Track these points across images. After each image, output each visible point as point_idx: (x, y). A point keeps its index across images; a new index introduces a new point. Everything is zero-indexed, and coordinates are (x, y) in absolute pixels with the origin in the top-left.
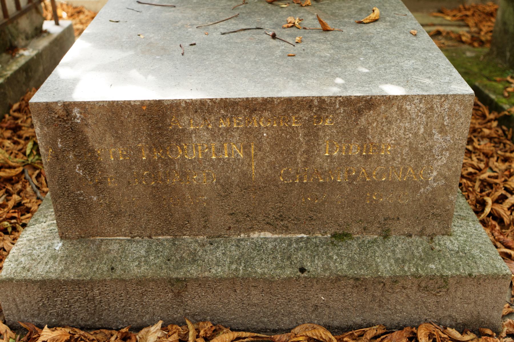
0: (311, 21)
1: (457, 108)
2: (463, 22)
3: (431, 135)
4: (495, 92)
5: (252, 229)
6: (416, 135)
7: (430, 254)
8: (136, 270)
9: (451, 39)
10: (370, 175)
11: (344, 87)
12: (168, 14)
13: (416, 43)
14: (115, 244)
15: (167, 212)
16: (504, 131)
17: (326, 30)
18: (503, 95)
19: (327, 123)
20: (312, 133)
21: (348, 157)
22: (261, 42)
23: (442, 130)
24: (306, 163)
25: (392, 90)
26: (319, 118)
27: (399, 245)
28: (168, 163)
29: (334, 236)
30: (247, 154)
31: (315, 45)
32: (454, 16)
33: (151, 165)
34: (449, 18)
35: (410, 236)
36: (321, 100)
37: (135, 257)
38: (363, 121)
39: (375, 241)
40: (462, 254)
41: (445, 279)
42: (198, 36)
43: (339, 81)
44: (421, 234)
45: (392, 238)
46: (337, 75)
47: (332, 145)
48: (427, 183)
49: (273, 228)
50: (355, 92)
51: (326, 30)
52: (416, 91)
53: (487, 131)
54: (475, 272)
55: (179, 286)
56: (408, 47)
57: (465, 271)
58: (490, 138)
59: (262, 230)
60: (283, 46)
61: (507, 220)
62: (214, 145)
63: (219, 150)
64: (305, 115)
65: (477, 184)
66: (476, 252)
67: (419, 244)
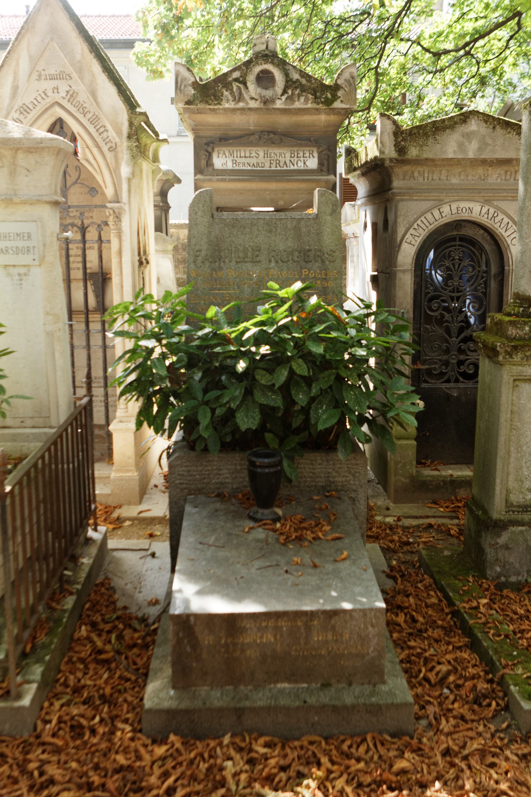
0: (307, 559)
1: (378, 614)
2: (454, 515)
3: (367, 628)
4: (454, 591)
5: (277, 681)
6: (360, 628)
7: (373, 694)
8: (217, 704)
9: (442, 532)
10: (339, 649)
11: (323, 604)
12: (221, 554)
13: (365, 576)
14: (203, 690)
15: (233, 674)
16: (455, 622)
17: (315, 566)
18: (458, 592)
19: (315, 622)
20: (308, 628)
21: (326, 641)
22: (280, 575)
23: (373, 626)
24: (305, 644)
25: (347, 606)
26: (311, 620)
27: (357, 689)
28: (235, 644)
29: (322, 685)
30: (275, 639)
31: (309, 577)
32: (447, 507)
33: (226, 645)
34: (442, 509)
35: (363, 684)
36: (312, 612)
37: (217, 697)
38: (333, 622)
39: (344, 688)
40: (391, 693)
41: (380, 706)
42: (244, 572)
43: (321, 601)
44: (369, 683)
45: (354, 686)
46: (320, 597)
47: (318, 634)
48: (368, 654)
49: (288, 680)
50: (328, 607)
51: (315, 566)
52: (358, 606)
53: (440, 622)
54: (395, 702)
55: (239, 712)
56: (359, 578)
57: (389, 701)
58: (443, 628)
59: (282, 682)
60: (292, 578)
61: (433, 681)
62: (259, 635)
63: (261, 637)
64: (304, 619)
65: (422, 660)
66: (397, 692)
67: (367, 689)
